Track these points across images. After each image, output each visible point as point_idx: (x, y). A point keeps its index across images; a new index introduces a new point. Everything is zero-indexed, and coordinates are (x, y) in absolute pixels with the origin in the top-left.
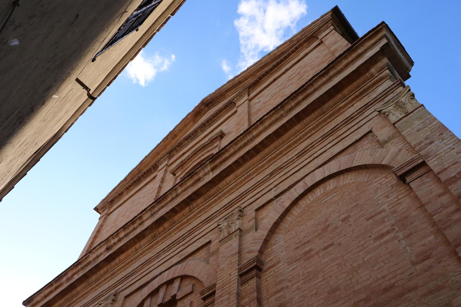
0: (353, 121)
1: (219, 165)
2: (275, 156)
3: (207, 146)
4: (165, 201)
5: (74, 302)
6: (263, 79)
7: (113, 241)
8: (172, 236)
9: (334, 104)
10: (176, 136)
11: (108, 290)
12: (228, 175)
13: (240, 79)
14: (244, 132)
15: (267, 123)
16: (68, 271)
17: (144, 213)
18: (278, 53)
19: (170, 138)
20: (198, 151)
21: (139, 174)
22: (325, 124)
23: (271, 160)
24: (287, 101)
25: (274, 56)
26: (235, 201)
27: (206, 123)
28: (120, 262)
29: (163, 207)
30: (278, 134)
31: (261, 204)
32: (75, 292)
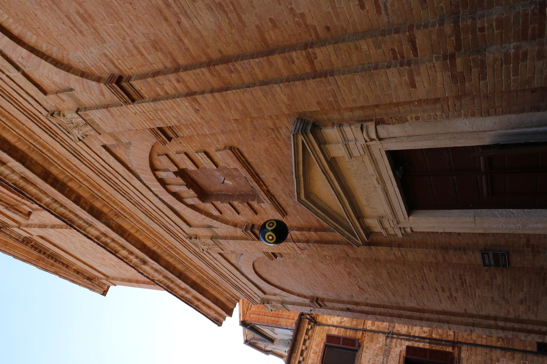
11: (188, 247)
17: (90, 236)
21: (43, 259)
29: (76, 215)
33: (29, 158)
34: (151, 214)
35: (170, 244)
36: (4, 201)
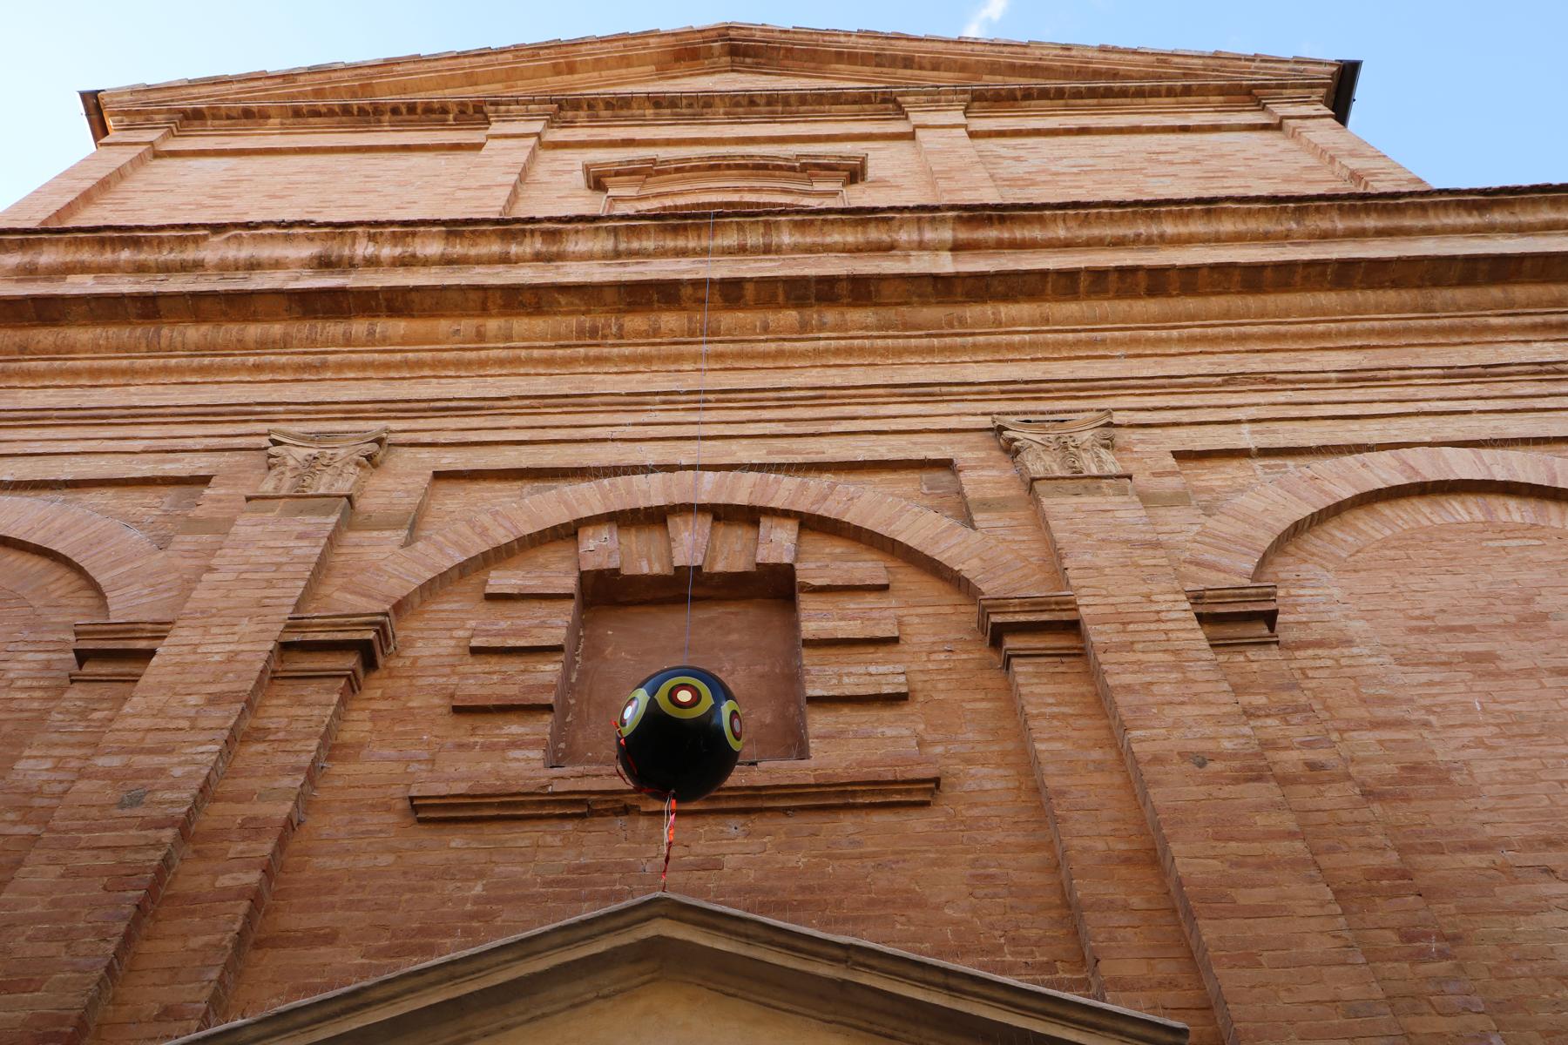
0: (1562, 383)
1: (988, 247)
2: (1217, 338)
3: (777, 173)
4: (699, 237)
5: (30, 374)
6: (1033, 102)
7: (364, 249)
8: (679, 371)
9: (1470, 306)
10: (571, 69)
11: (307, 413)
12: (1009, 297)
13: (914, 51)
14: (1137, 203)
15: (1227, 226)
16: (50, 241)
17: (580, 226)
18: (1100, 63)
19: (545, 59)
20: (729, 167)
21: (354, 95)
22: (1422, 341)
23: (1197, 340)
24: (1325, 203)
25: (1081, 62)
26: (1058, 390)
27: (763, 101)
28: (371, 339)
29: (682, 253)
30: (1253, 278)
31: (1198, 447)
32: (51, 339)
33: (933, 301)
34: (560, 410)
35: (329, 375)
36: (670, 173)
